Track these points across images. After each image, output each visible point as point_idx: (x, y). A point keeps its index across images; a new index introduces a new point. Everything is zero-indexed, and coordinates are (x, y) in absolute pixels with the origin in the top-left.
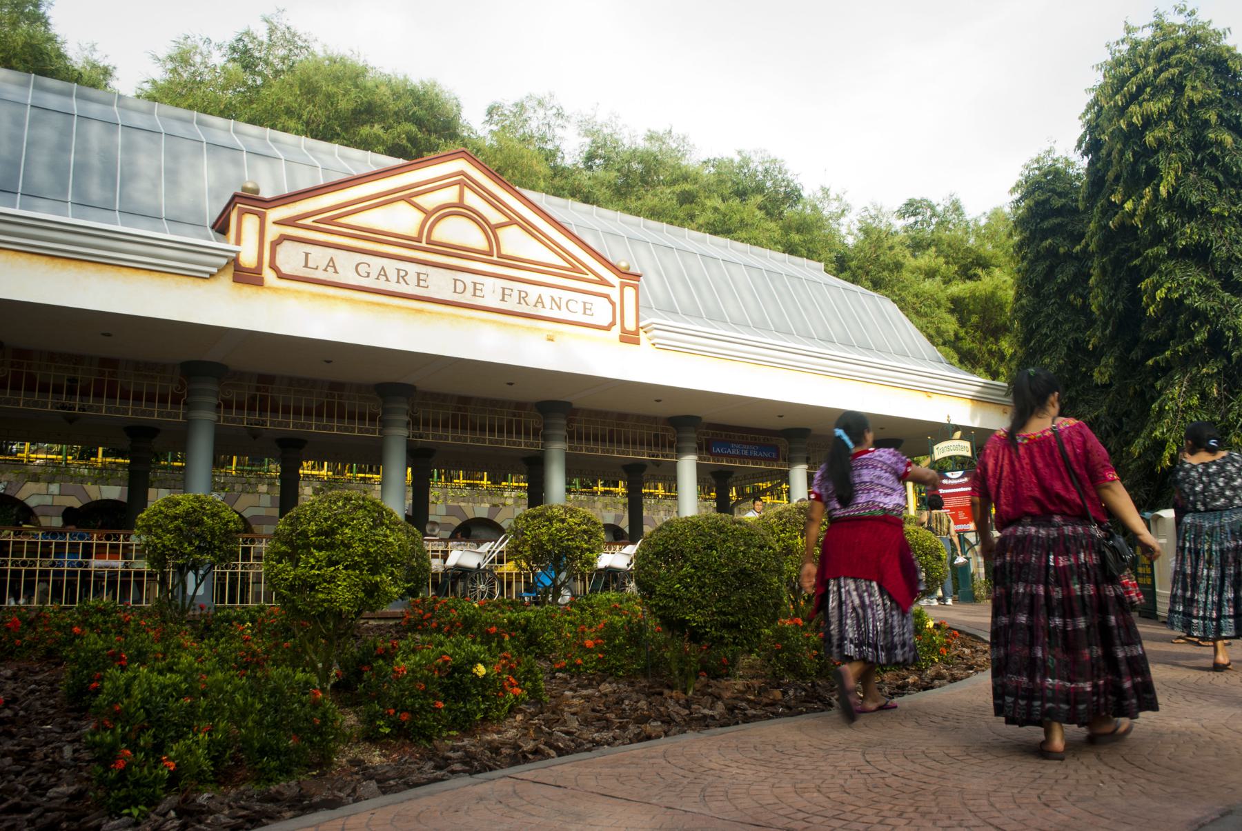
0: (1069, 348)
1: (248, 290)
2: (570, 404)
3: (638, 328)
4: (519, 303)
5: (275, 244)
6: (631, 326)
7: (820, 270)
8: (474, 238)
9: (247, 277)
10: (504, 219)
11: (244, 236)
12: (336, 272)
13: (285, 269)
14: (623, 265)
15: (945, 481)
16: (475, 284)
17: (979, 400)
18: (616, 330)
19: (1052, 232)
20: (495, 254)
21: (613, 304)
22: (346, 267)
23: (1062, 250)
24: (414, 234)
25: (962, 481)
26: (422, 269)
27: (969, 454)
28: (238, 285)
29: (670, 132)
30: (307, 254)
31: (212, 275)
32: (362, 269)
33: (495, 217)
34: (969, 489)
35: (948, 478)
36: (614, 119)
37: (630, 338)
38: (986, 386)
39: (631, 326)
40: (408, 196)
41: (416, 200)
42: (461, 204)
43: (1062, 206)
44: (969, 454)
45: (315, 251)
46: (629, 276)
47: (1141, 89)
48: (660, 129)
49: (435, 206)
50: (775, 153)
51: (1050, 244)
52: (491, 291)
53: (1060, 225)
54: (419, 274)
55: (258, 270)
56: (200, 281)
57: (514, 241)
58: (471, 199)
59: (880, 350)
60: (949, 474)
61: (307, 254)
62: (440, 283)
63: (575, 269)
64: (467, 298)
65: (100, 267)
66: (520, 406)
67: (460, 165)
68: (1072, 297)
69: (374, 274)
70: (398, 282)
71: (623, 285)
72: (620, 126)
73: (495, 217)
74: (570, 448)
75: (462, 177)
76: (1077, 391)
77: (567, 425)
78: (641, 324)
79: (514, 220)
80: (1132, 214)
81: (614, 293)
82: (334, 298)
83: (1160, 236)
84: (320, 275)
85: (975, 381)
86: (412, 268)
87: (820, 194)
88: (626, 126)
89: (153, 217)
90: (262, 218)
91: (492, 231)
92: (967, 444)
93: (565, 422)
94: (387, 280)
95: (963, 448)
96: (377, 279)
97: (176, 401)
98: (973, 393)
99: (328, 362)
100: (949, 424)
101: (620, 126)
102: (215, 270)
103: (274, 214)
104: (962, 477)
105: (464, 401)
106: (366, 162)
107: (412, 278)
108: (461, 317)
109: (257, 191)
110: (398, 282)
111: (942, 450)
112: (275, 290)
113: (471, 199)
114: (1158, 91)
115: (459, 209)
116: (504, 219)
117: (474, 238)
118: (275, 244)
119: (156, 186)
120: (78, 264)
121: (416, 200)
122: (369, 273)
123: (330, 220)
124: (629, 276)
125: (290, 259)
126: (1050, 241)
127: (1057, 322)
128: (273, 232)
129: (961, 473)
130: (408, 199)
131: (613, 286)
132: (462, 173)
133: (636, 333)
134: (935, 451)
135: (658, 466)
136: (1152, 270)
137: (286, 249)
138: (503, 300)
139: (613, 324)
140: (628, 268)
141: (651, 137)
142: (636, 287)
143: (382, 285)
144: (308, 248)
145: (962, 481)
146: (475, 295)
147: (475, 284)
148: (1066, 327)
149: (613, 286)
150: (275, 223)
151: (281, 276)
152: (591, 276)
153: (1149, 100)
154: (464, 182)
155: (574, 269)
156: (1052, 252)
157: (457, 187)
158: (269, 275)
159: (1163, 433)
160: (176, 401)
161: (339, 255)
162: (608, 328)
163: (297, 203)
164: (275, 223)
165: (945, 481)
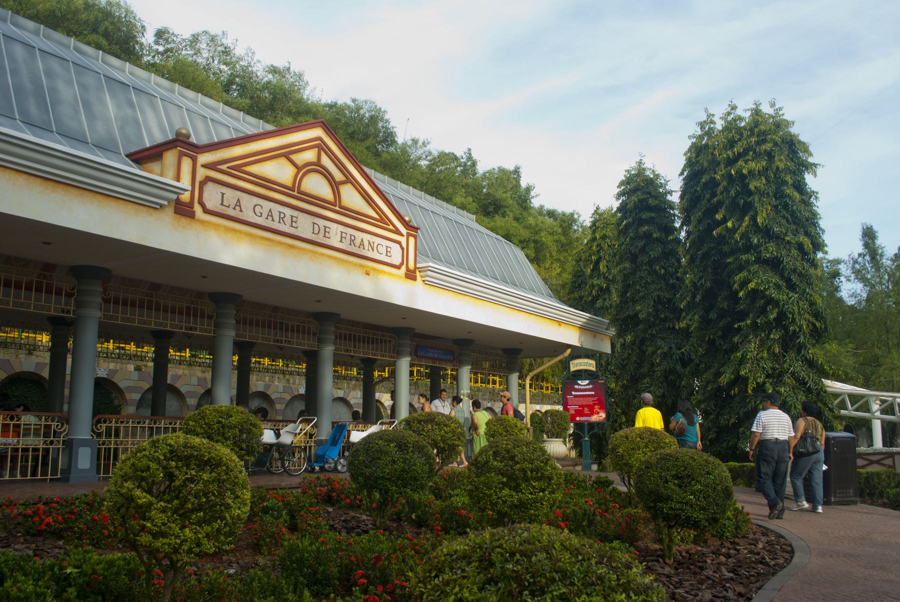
0: (654, 301)
1: (184, 221)
2: (240, 296)
3: (416, 268)
4: (350, 244)
5: (203, 184)
6: (411, 266)
7: (473, 221)
8: (323, 189)
9: (184, 210)
10: (343, 178)
11: (182, 176)
12: (241, 211)
13: (209, 205)
14: (407, 219)
15: (576, 387)
16: (325, 227)
17: (583, 328)
18: (404, 268)
19: (647, 222)
20: (336, 205)
21: (402, 248)
22: (249, 207)
23: (655, 236)
24: (289, 183)
25: (588, 387)
26: (295, 213)
27: (594, 369)
28: (178, 216)
29: (289, 68)
30: (223, 194)
31: (162, 206)
32: (258, 209)
33: (338, 176)
34: (593, 393)
35: (579, 385)
36: (250, 54)
37: (411, 275)
38: (589, 320)
39: (411, 266)
40: (286, 153)
41: (293, 157)
42: (318, 163)
43: (656, 206)
44: (594, 369)
45: (229, 192)
46: (412, 228)
47: (746, 151)
48: (280, 64)
49: (303, 163)
50: (381, 104)
51: (647, 230)
52: (335, 235)
53: (652, 218)
54: (292, 217)
55: (190, 205)
56: (151, 210)
57: (351, 197)
58: (326, 161)
59: (522, 287)
60: (579, 382)
61: (223, 194)
62: (305, 226)
63: (383, 221)
64: (320, 239)
65: (81, 192)
66: (200, 295)
67: (318, 132)
68: (657, 268)
69: (264, 215)
70: (279, 222)
71: (409, 235)
72: (255, 61)
73: (338, 176)
74: (105, 316)
75: (319, 142)
76: (656, 331)
77: (104, 292)
78: (418, 266)
79: (349, 179)
80: (734, 230)
81: (403, 240)
82: (240, 232)
83: (748, 248)
84: (230, 212)
85: (582, 317)
86: (288, 212)
87: (410, 143)
88: (259, 61)
89: (82, 141)
90: (194, 160)
91: (335, 185)
92: (593, 362)
93: (102, 290)
94: (273, 220)
95: (590, 365)
96: (267, 218)
97: (69, 295)
98: (581, 323)
99: (204, 277)
100: (582, 347)
101: (255, 61)
102: (166, 203)
103: (205, 158)
104: (588, 384)
105: (276, 309)
106: (197, 102)
107: (288, 220)
108: (317, 253)
109: (188, 136)
110: (279, 222)
111: (577, 365)
112: (202, 222)
113: (326, 161)
114: (757, 156)
115: (317, 168)
116: (343, 178)
117: (323, 189)
118: (203, 184)
119: (77, 112)
120: (64, 187)
121: (293, 157)
122: (261, 213)
123: (238, 168)
124: (412, 228)
125: (212, 196)
126: (646, 228)
127: (646, 283)
128: (202, 173)
129: (587, 382)
130: (287, 156)
131: (403, 235)
132: (320, 139)
133: (414, 272)
134: (571, 366)
135: (189, 338)
136: (741, 269)
137: (210, 188)
138: (341, 241)
139: (402, 264)
140: (410, 221)
141: (274, 70)
142: (415, 237)
143: (269, 223)
144: (224, 190)
145: (588, 387)
146: (325, 236)
147: (325, 227)
148: (652, 287)
149: (403, 235)
150: (204, 166)
151: (206, 211)
152: (391, 227)
153: (752, 160)
154: (322, 147)
155: (382, 220)
156: (648, 236)
157: (316, 150)
158: (198, 209)
159: (746, 373)
160: (69, 295)
161: (244, 197)
162: (398, 267)
163: (217, 151)
164: (204, 166)
165: (576, 387)
